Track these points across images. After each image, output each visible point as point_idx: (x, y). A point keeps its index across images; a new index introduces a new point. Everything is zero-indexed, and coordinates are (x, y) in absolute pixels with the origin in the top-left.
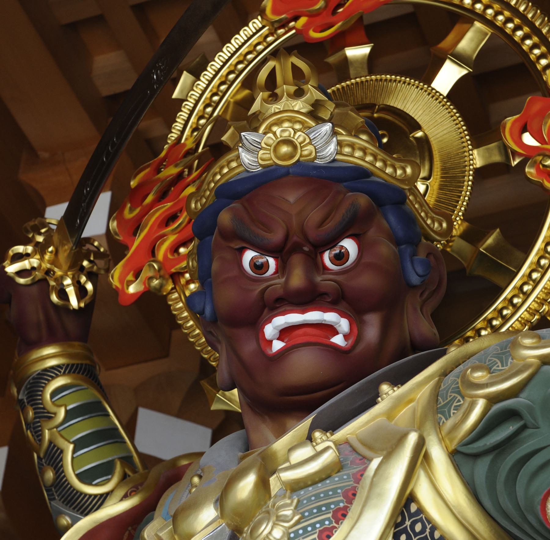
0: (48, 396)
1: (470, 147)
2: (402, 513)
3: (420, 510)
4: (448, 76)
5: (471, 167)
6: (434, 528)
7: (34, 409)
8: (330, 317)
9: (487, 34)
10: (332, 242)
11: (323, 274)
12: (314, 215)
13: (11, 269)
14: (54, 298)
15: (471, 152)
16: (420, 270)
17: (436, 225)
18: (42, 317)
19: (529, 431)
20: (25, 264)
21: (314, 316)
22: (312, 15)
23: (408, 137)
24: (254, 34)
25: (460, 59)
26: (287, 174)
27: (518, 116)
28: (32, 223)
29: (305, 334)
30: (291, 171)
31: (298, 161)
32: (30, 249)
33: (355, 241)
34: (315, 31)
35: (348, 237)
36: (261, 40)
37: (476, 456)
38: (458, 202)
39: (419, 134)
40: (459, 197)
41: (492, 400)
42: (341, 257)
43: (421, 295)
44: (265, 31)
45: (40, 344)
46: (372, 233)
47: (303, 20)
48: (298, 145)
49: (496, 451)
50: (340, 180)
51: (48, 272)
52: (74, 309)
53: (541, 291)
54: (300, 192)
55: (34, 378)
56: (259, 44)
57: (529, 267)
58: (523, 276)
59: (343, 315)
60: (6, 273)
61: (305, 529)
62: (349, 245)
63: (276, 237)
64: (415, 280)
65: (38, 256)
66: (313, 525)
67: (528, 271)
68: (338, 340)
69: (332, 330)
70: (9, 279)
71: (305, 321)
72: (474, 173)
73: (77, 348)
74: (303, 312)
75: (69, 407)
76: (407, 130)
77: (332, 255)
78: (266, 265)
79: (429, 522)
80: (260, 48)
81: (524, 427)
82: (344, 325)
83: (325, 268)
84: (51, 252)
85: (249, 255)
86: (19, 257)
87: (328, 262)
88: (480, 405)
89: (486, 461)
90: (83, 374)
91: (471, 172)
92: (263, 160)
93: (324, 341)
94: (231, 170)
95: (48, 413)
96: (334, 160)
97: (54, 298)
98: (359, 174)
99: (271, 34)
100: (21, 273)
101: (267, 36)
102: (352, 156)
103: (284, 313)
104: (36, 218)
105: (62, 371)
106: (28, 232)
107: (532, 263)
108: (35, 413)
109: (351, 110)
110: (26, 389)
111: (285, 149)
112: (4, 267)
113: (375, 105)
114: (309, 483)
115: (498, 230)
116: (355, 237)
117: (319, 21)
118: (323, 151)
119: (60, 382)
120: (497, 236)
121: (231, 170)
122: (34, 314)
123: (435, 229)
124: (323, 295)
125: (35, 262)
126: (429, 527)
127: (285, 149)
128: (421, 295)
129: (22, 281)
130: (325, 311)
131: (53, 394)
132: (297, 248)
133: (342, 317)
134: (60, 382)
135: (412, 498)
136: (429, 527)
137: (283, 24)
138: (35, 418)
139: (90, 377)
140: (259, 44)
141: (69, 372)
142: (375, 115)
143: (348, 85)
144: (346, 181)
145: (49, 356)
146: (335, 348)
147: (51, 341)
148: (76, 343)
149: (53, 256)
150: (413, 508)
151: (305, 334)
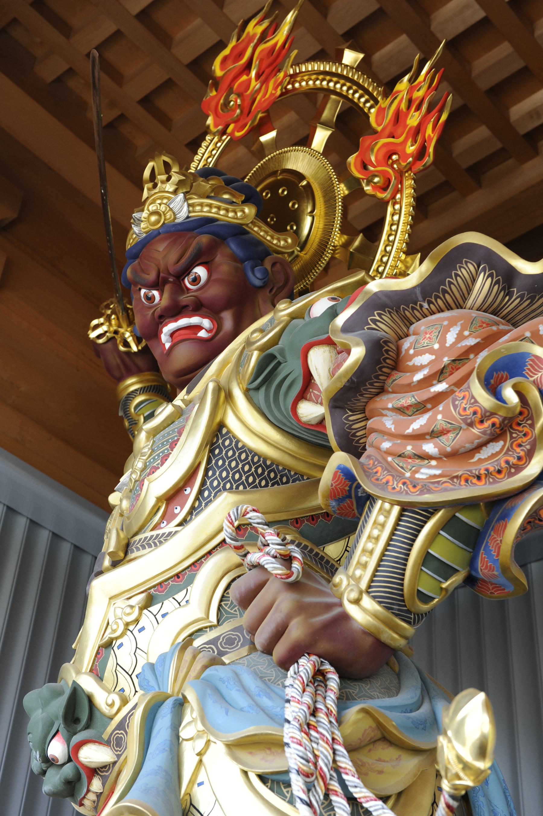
0: (133, 410)
1: (337, 183)
2: (217, 436)
3: (229, 432)
4: (321, 136)
5: (339, 196)
6: (238, 441)
7: (128, 420)
8: (195, 320)
9: (339, 102)
10: (187, 270)
11: (188, 293)
12: (173, 256)
13: (93, 335)
14: (122, 348)
15: (338, 186)
16: (259, 275)
17: (282, 243)
18: (119, 361)
19: (282, 365)
20: (99, 331)
21: (183, 322)
22: (236, 121)
23: (298, 187)
24: (210, 144)
25: (326, 125)
26: (159, 234)
27: (357, 153)
28: (105, 303)
29: (180, 335)
30: (160, 231)
31: (164, 223)
32: (102, 320)
33: (204, 267)
34: (238, 132)
35: (198, 265)
36: (214, 147)
37: (257, 389)
38: (334, 222)
39: (304, 183)
40: (335, 218)
41: (262, 349)
42: (196, 280)
43: (271, 291)
44: (216, 139)
45: (121, 379)
46: (218, 258)
47: (232, 127)
48: (162, 213)
49: (267, 383)
50: (192, 229)
51: (116, 332)
52: (135, 352)
53: (389, 268)
54: (165, 244)
55: (124, 401)
56: (213, 150)
57: (380, 254)
58: (378, 261)
59: (203, 317)
60: (90, 338)
61: (154, 458)
62: (201, 271)
63: (151, 276)
64: (257, 283)
65: (107, 324)
66: (158, 455)
67: (380, 257)
68: (202, 334)
69: (199, 328)
70: (93, 342)
71: (178, 326)
72: (342, 200)
73: (148, 376)
74: (176, 321)
75: (145, 415)
76: (296, 181)
77: (190, 280)
78: (153, 297)
79: (235, 438)
80: (214, 152)
81: (279, 363)
82: (206, 323)
83: (188, 289)
84: (114, 319)
85: (143, 291)
86: (97, 327)
87: (189, 285)
88: (256, 354)
89: (263, 390)
90: (152, 392)
91: (340, 200)
92: (144, 229)
93: (194, 336)
94: (134, 239)
95: (135, 421)
96: (188, 217)
97: (122, 348)
98: (207, 222)
99: (219, 141)
100: (99, 337)
101: (217, 143)
102: (202, 211)
103: (166, 325)
104: (108, 299)
105: (138, 392)
106: (102, 309)
107: (381, 251)
108: (129, 422)
109: (202, 181)
110: (121, 409)
111: (153, 218)
112: (89, 335)
113: (277, 171)
114: (162, 429)
115: (361, 234)
116: (205, 264)
117: (240, 124)
118: (180, 213)
119: (140, 398)
120: (361, 239)
121: (134, 239)
122: (114, 360)
123: (281, 245)
124: (186, 307)
125: (104, 328)
126: (234, 441)
127: (153, 218)
128: (271, 291)
129: (101, 341)
130: (190, 317)
131: (136, 408)
132: (165, 281)
133: (203, 318)
134: (140, 398)
135: (222, 425)
136: (234, 441)
137: (223, 132)
138: (130, 425)
139: (158, 393)
140: (213, 150)
141: (143, 392)
142: (279, 178)
143: (264, 162)
144: (196, 229)
145: (132, 384)
146: (201, 340)
147: (130, 374)
148: (146, 373)
149: (117, 321)
150: (224, 431)
151: (180, 335)
